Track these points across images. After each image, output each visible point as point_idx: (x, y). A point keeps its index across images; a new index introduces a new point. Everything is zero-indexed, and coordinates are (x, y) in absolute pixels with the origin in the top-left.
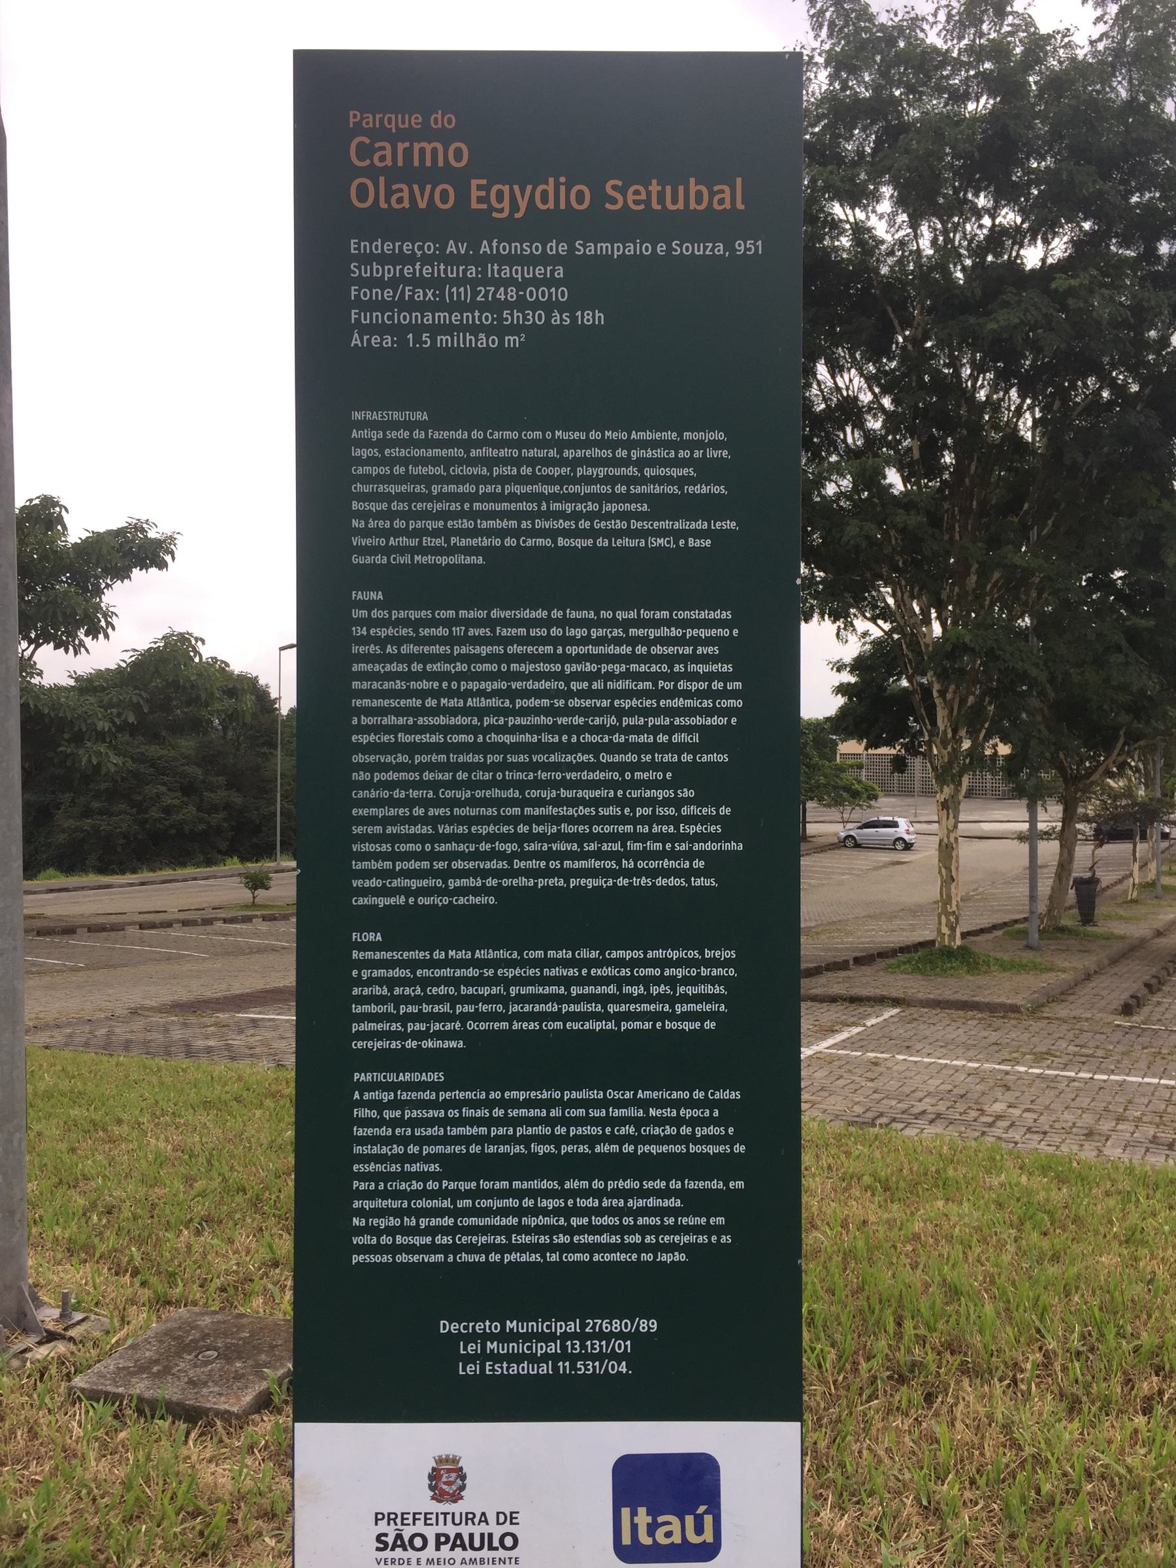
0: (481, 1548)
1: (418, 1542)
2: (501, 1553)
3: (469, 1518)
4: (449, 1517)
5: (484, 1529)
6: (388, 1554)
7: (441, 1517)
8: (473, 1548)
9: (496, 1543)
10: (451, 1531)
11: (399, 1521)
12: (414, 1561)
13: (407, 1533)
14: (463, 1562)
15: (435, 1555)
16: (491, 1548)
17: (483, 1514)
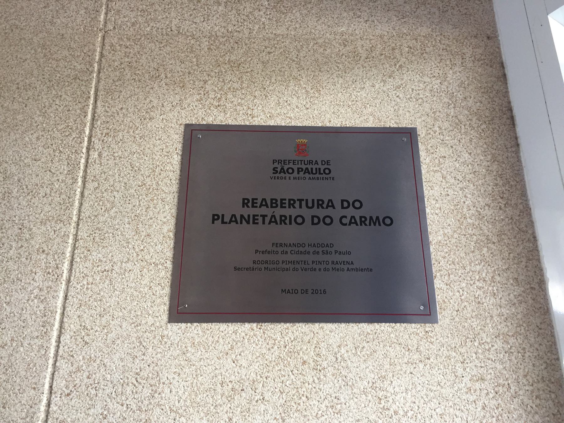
2: (324, 176)
3: (310, 162)
4: (303, 162)
5: (316, 166)
7: (300, 162)
8: (313, 173)
10: (304, 167)
11: (283, 163)
15: (297, 176)
16: (320, 173)
17: (316, 161)
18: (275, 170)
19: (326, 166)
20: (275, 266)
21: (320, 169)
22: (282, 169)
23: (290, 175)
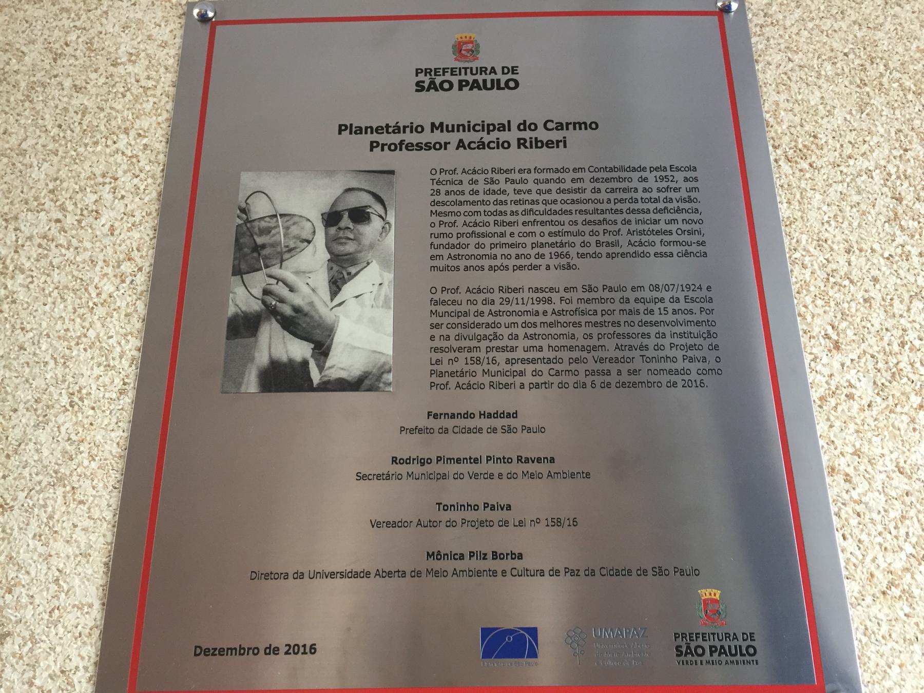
0: (736, 654)
1: (446, 86)
2: (748, 658)
3: (483, 70)
4: (469, 71)
5: (493, 76)
6: (683, 658)
7: (463, 71)
8: (731, 655)
9: (502, 85)
10: (470, 78)
11: (433, 73)
12: (699, 662)
13: (438, 80)
14: (727, 663)
15: (711, 659)
16: (742, 655)
17: (735, 634)
18: (420, 87)
19: (510, 76)
20: (448, 177)
21: (498, 81)
22: (688, 647)
23: (701, 658)
